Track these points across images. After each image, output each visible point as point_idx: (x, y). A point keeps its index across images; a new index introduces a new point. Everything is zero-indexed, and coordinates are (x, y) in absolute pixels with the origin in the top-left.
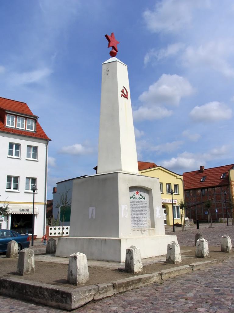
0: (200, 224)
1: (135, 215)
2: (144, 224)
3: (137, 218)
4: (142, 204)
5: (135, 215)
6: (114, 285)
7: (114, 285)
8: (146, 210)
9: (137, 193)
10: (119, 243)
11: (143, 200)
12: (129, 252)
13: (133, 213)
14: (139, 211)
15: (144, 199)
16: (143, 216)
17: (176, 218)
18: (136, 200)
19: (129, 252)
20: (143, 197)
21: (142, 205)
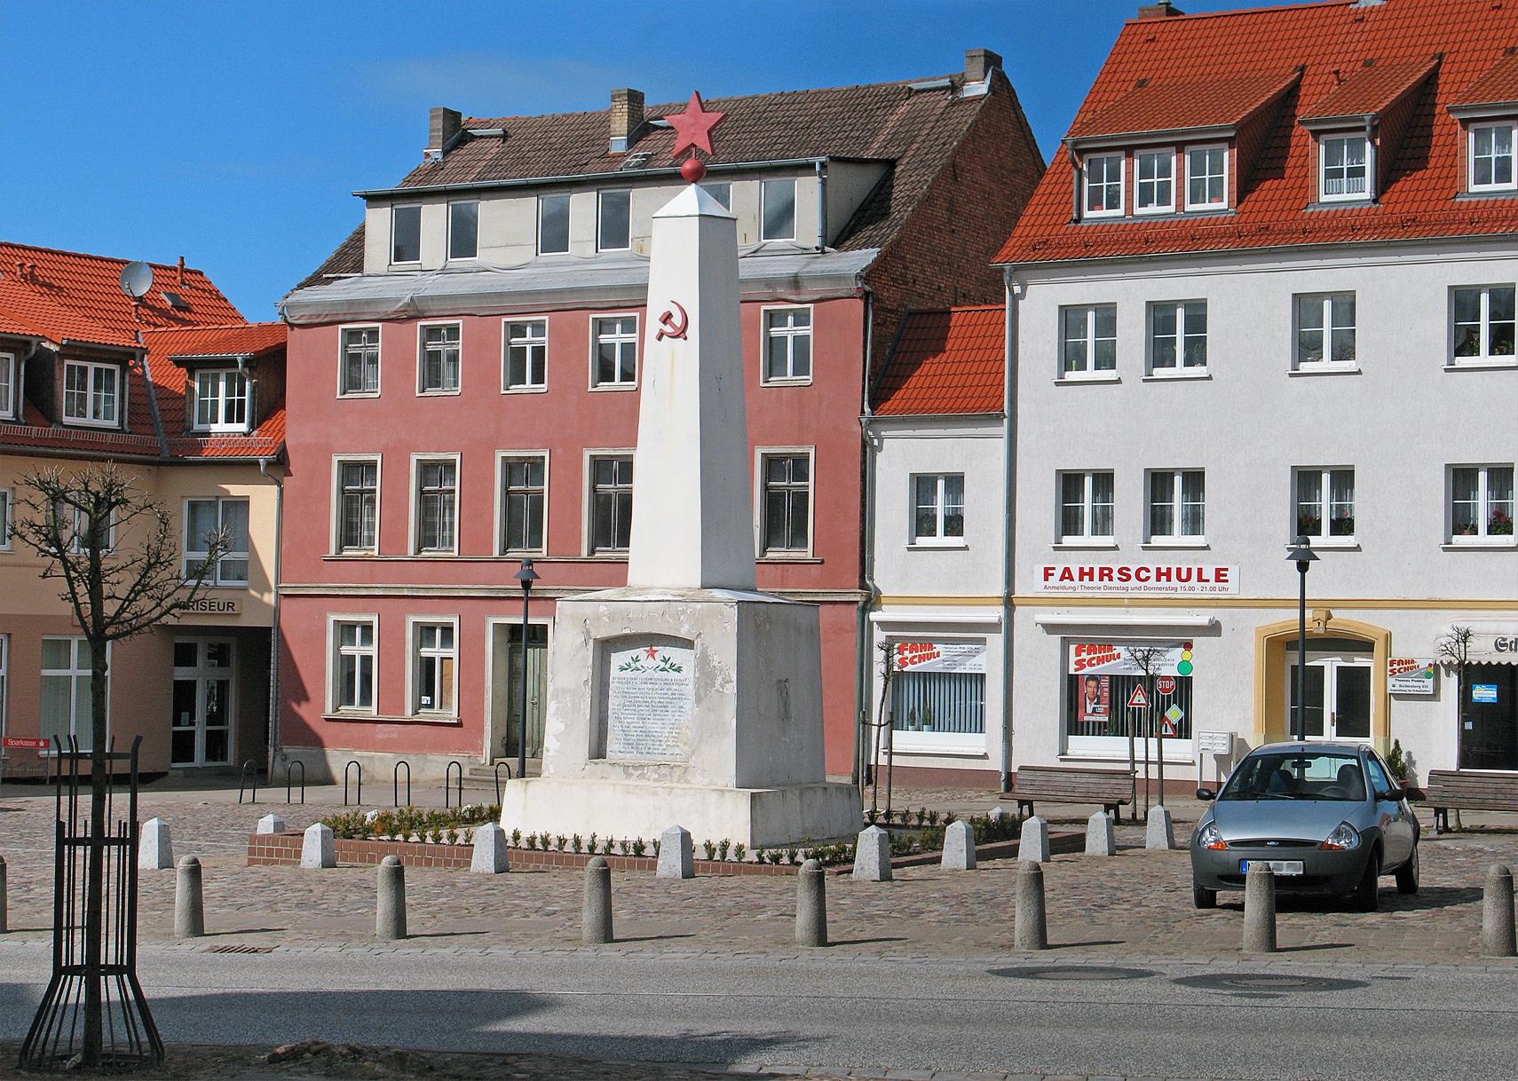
0: (244, 790)
1: (630, 720)
2: (664, 747)
3: (639, 730)
4: (668, 687)
5: (630, 720)
6: (167, 432)
7: (167, 432)
8: (681, 705)
9: (652, 654)
10: (1334, 353)
11: (673, 675)
12: (1397, 742)
13: (626, 714)
14: (650, 708)
15: (679, 670)
16: (664, 724)
17: (1143, 707)
18: (644, 675)
19: (1397, 742)
20: (672, 665)
21: (665, 691)
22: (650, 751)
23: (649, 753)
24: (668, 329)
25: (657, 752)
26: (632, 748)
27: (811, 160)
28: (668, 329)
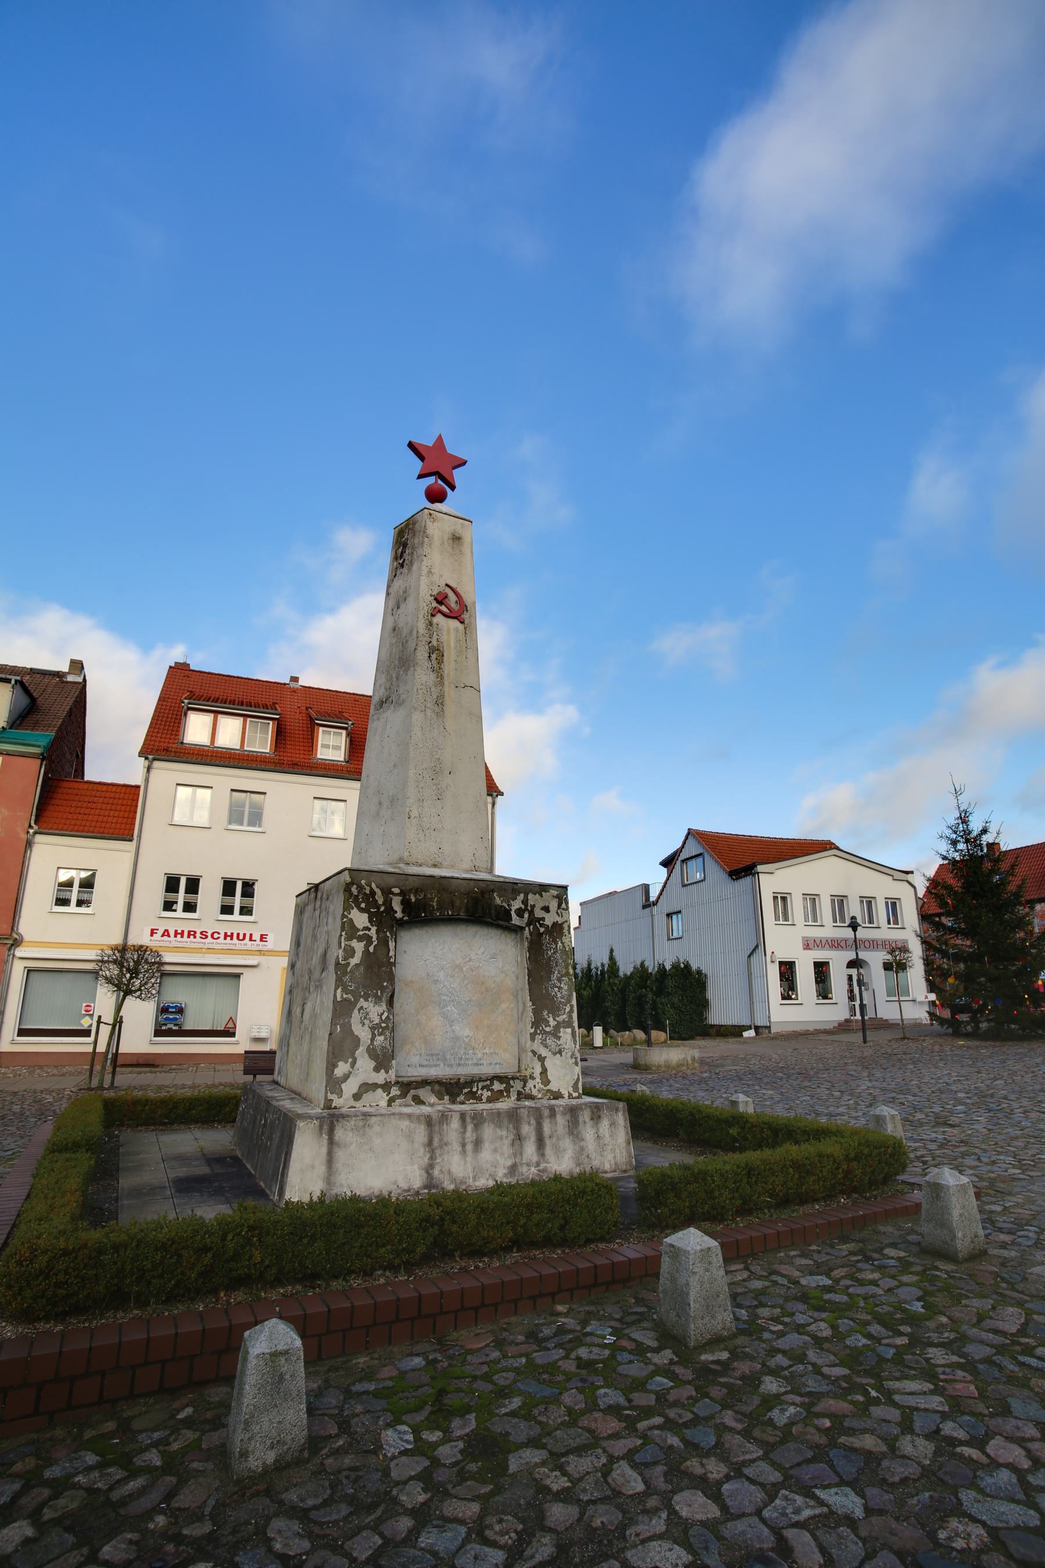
2: (480, 1055)
23: (459, 1065)
27: (8, 677)
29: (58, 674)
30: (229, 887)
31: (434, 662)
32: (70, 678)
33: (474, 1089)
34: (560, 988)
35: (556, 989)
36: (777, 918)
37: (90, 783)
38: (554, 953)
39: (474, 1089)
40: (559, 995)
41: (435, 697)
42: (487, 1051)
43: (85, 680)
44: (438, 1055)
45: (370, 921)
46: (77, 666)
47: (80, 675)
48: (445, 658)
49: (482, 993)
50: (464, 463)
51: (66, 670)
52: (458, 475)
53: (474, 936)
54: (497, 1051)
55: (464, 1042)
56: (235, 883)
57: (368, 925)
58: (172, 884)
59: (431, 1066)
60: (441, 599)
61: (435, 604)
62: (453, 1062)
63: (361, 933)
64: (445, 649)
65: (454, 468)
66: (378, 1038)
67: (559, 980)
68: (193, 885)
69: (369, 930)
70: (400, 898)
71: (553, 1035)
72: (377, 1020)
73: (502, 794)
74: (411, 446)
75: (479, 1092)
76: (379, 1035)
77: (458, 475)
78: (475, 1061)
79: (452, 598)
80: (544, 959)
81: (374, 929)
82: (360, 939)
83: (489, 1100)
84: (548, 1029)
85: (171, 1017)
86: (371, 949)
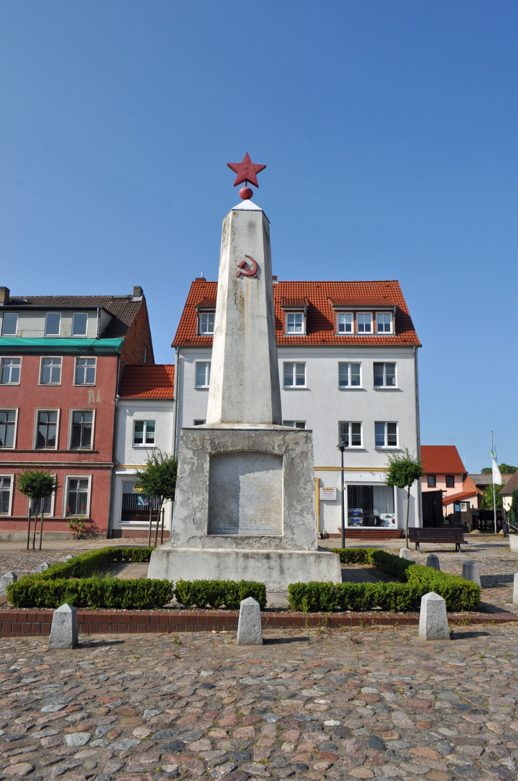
2: (259, 525)
22: (248, 528)
23: (247, 529)
24: (243, 271)
25: (253, 528)
26: (235, 526)
28: (243, 271)
29: (129, 298)
30: (379, 425)
31: (239, 305)
32: (135, 299)
33: (251, 542)
34: (305, 489)
35: (303, 489)
36: (379, 442)
37: (158, 366)
38: (302, 469)
39: (251, 542)
40: (304, 492)
41: (239, 326)
42: (263, 522)
43: (144, 299)
44: (234, 524)
45: (194, 454)
46: (140, 291)
47: (140, 296)
48: (245, 302)
49: (260, 491)
50: (265, 167)
51: (132, 293)
52: (260, 177)
53: (256, 460)
54: (269, 523)
55: (249, 517)
56: (348, 424)
57: (192, 456)
58: (343, 427)
59: (231, 529)
60: (244, 266)
61: (239, 269)
62: (243, 527)
63: (189, 461)
64: (245, 296)
65: (257, 173)
66: (198, 514)
67: (305, 484)
68: (357, 426)
69: (194, 459)
70: (210, 442)
71: (300, 515)
72: (197, 505)
73: (421, 346)
74: (229, 165)
75: (254, 544)
76: (199, 512)
77: (260, 177)
78: (255, 528)
79: (250, 262)
80: (295, 472)
81: (196, 458)
82: (188, 463)
83: (258, 548)
84: (296, 511)
85: (355, 519)
86: (194, 469)
